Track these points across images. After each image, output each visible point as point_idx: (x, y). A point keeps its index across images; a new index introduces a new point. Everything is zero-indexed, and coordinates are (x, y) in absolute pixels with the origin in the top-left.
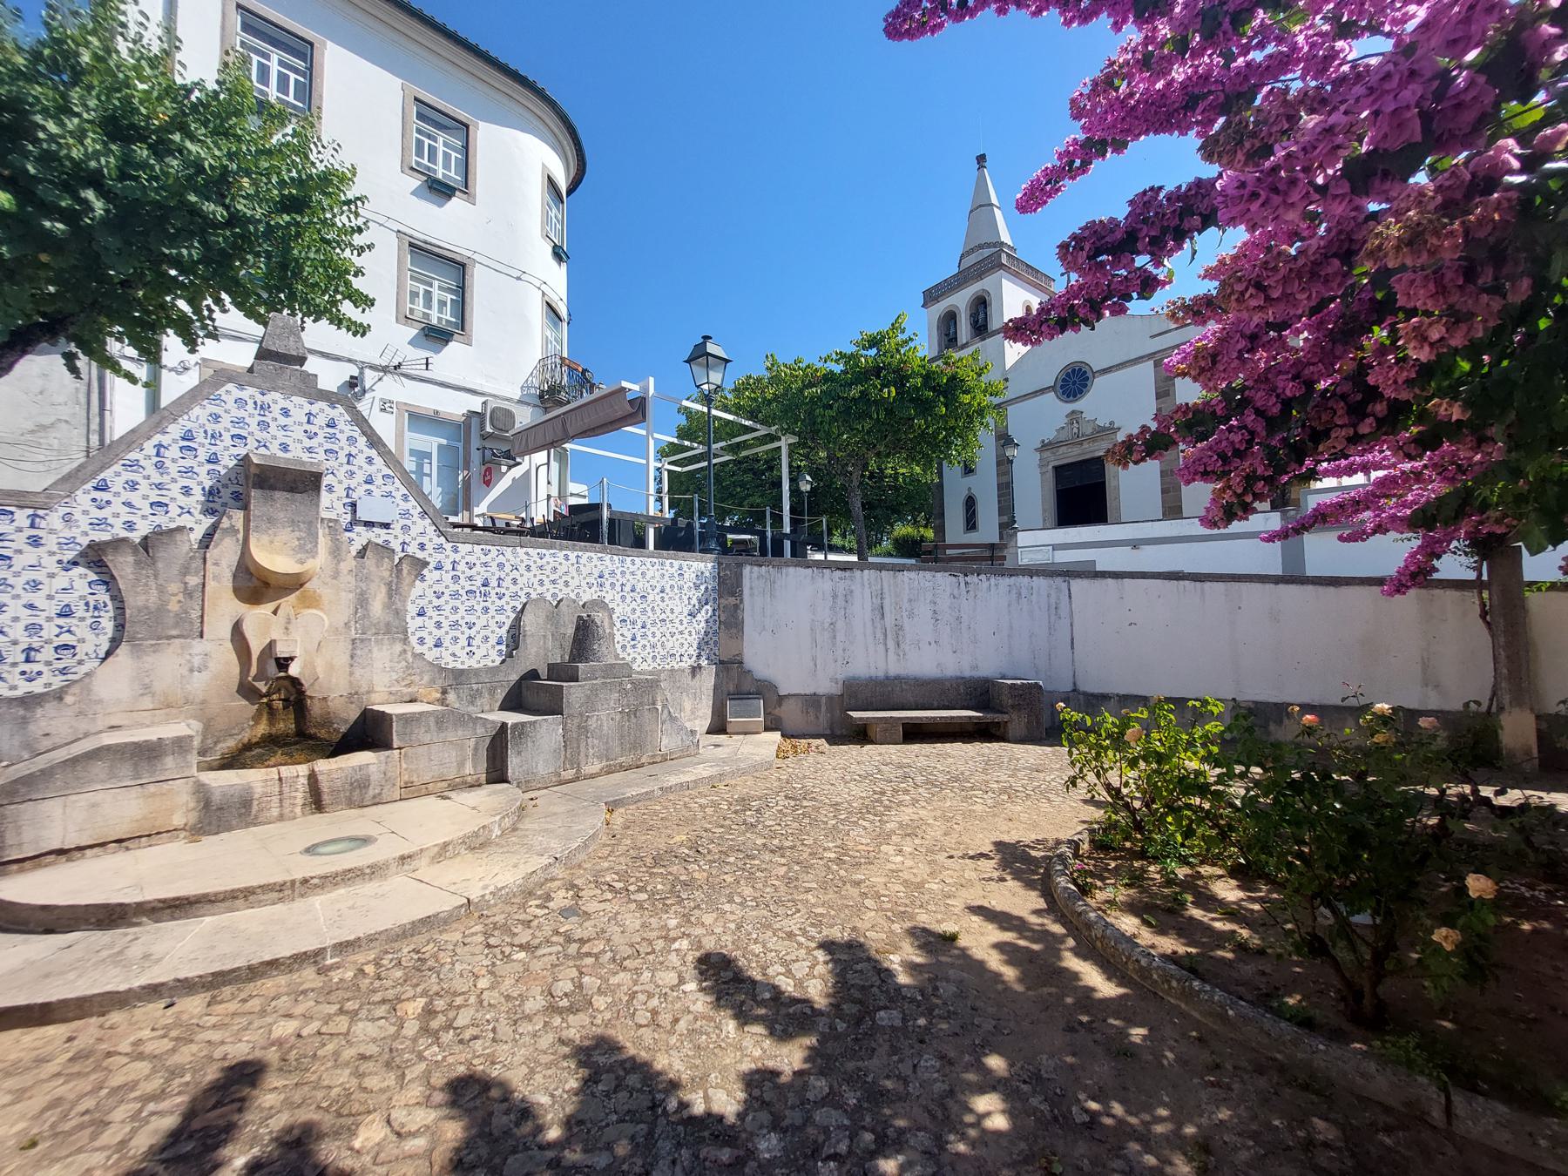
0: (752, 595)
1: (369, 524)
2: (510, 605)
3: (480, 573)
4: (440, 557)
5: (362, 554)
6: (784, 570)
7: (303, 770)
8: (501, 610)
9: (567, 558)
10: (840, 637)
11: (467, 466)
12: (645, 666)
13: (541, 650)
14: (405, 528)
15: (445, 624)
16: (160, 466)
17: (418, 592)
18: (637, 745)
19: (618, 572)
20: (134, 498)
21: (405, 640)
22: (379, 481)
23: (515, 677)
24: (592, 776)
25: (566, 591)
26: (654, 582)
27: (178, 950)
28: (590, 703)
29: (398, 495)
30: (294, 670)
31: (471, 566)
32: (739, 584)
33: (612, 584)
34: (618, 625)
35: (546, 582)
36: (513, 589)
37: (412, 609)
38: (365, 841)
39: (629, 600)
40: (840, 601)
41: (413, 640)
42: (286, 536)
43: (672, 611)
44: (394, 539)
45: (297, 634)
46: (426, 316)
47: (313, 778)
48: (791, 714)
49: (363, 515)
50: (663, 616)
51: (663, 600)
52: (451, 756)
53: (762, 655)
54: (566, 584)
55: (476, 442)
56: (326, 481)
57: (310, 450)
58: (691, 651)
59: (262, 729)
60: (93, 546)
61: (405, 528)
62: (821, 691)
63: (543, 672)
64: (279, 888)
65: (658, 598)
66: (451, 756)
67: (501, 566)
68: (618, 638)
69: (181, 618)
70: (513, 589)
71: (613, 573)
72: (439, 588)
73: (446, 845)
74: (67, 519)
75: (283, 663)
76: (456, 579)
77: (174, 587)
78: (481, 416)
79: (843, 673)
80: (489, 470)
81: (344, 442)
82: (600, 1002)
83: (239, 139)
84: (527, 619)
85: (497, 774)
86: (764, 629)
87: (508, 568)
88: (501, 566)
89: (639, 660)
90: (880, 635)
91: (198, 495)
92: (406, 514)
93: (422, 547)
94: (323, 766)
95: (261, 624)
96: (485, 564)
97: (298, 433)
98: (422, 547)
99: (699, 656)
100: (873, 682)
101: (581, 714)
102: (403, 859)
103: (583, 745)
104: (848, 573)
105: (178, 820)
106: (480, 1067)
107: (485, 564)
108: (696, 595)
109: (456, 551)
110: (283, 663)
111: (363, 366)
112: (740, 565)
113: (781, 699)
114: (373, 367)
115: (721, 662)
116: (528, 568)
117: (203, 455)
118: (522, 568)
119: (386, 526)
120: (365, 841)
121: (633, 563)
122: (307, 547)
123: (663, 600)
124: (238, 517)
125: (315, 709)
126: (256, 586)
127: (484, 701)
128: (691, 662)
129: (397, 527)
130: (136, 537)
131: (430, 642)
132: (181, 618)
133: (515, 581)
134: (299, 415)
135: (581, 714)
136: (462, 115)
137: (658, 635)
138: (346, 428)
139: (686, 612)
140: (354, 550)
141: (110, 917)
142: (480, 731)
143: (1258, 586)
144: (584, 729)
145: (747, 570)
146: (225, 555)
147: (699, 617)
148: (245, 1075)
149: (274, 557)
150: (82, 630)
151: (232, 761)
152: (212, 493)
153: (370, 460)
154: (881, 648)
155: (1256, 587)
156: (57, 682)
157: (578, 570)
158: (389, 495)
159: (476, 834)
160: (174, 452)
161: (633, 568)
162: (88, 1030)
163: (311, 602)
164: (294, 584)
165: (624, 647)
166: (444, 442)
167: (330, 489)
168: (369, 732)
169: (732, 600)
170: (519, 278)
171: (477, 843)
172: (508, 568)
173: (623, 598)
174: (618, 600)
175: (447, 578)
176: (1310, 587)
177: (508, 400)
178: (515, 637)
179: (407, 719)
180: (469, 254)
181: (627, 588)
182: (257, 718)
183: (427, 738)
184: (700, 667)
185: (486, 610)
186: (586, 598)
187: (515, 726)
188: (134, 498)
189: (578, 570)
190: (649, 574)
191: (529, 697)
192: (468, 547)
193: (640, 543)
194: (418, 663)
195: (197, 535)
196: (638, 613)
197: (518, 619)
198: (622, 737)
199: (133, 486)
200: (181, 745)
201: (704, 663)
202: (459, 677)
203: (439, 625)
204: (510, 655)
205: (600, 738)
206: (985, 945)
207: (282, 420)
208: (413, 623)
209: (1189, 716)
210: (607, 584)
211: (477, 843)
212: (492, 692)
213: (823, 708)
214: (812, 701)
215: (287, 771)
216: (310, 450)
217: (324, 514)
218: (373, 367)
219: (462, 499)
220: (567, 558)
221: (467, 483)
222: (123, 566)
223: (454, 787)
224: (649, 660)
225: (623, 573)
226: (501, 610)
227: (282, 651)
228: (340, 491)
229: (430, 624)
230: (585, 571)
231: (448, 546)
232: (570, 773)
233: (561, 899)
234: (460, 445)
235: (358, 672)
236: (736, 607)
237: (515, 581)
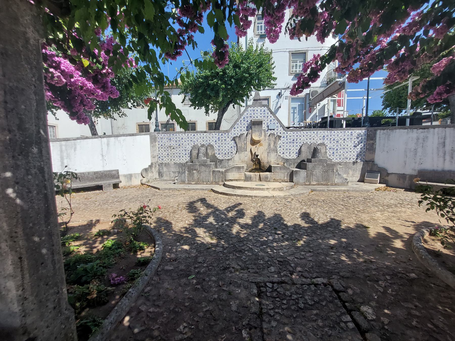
0: (380, 140)
1: (271, 130)
3: (292, 138)
4: (284, 135)
5: (269, 136)
6: (394, 131)
7: (258, 174)
8: (297, 146)
9: (314, 133)
10: (419, 154)
11: (305, 109)
12: (337, 161)
13: (306, 155)
14: (277, 130)
15: (285, 149)
16: (241, 124)
17: (280, 142)
18: (327, 180)
19: (329, 135)
20: (238, 129)
21: (277, 152)
22: (272, 121)
23: (299, 161)
24: (314, 185)
25: (313, 141)
26: (341, 137)
27: (239, 192)
28: (314, 168)
29: (276, 123)
30: (259, 157)
31: (290, 136)
33: (327, 139)
34: (328, 149)
35: (308, 139)
36: (300, 141)
37: (279, 146)
38: (264, 185)
39: (332, 142)
40: (421, 141)
41: (279, 153)
42: (257, 133)
43: (347, 145)
44: (275, 132)
45: (259, 151)
46: (296, 71)
47: (260, 175)
48: (392, 179)
49: (270, 128)
50: (344, 147)
51: (344, 142)
52: (282, 175)
53: (381, 159)
54: (314, 139)
55: (308, 102)
56: (263, 122)
57: (261, 117)
58: (354, 157)
59: (254, 167)
60: (234, 137)
61: (277, 130)
62: (407, 173)
63: (306, 160)
64: (250, 188)
65: (342, 142)
66: (282, 175)
67: (297, 136)
68: (328, 153)
69: (244, 148)
70: (300, 141)
71: (328, 136)
72: (284, 142)
73: (275, 188)
74: (231, 134)
75: (257, 156)
76: (287, 139)
77: (243, 143)
78: (309, 94)
79: (418, 167)
80: (311, 109)
81: (266, 114)
82: (283, 211)
84: (303, 148)
85: (291, 180)
86: (384, 151)
87: (299, 136)
88: (297, 136)
89: (335, 159)
90: (441, 154)
91: (246, 128)
92: (277, 127)
93: (280, 133)
94: (261, 173)
95: (253, 148)
96: (293, 136)
97: (259, 114)
98: (280, 133)
99: (357, 159)
100: (435, 172)
101: (311, 170)
102: (267, 189)
103: (311, 178)
104: (426, 130)
105: (243, 179)
106: (263, 211)
107: (293, 136)
109: (287, 133)
110: (257, 156)
111: (281, 89)
112: (376, 130)
113: (388, 174)
114: (284, 89)
115: (366, 161)
116: (304, 136)
117: (246, 121)
118: (302, 136)
119: (274, 130)
120: (264, 185)
121: (334, 132)
122: (260, 135)
123: (344, 142)
124: (251, 130)
125: (262, 164)
126: (254, 143)
127: (292, 166)
128: (354, 160)
129: (276, 129)
130: (238, 136)
131: (282, 153)
132: (244, 148)
133: (300, 139)
134: (259, 111)
135: (311, 170)
137: (342, 152)
138: (267, 111)
139: (353, 145)
140: (269, 134)
141: (233, 187)
142: (288, 171)
144: (312, 174)
145: (378, 132)
146: (249, 137)
147: (358, 147)
148: (241, 204)
149: (256, 138)
150: (233, 150)
151: (250, 171)
152: (247, 127)
153: (271, 117)
154: (441, 159)
156: (231, 157)
157: (317, 135)
158: (274, 123)
159: (280, 188)
160: (242, 121)
161: (334, 134)
162: (230, 197)
163: (261, 145)
165: (330, 155)
166: (300, 103)
167: (264, 123)
168: (269, 170)
169: (372, 142)
170: (321, 50)
171: (281, 189)
172: (299, 136)
173: (331, 142)
174: (329, 142)
175: (285, 139)
177: (317, 87)
178: (300, 152)
179: (275, 167)
180: (306, 49)
181: (332, 139)
182: (254, 165)
183: (278, 171)
184: (357, 162)
185: (293, 146)
186: (319, 142)
187: (295, 171)
188: (238, 129)
189: (317, 135)
190: (340, 135)
191: (302, 166)
192: (290, 132)
193: (341, 126)
194: (279, 157)
195: (245, 135)
196: (335, 146)
197: (301, 148)
198: (323, 177)
199: (238, 127)
200: (243, 167)
201: (359, 161)
202: (287, 160)
203: (283, 149)
204: (298, 156)
205: (316, 177)
207: (257, 112)
208: (279, 149)
210: (326, 139)
211: (281, 189)
212: (294, 164)
213: (407, 179)
214: (402, 176)
215: (256, 173)
216: (261, 117)
217: (263, 129)
218: (284, 89)
219: (304, 118)
220: (314, 133)
221: (305, 113)
222: (237, 140)
223: (283, 181)
224: (338, 159)
225: (331, 135)
226: (297, 146)
227: (257, 154)
228: (266, 124)
229: (282, 149)
230: (319, 136)
231: (286, 132)
232: (308, 182)
233: (289, 200)
234: (304, 103)
235: (269, 158)
236: (373, 144)
237: (300, 139)
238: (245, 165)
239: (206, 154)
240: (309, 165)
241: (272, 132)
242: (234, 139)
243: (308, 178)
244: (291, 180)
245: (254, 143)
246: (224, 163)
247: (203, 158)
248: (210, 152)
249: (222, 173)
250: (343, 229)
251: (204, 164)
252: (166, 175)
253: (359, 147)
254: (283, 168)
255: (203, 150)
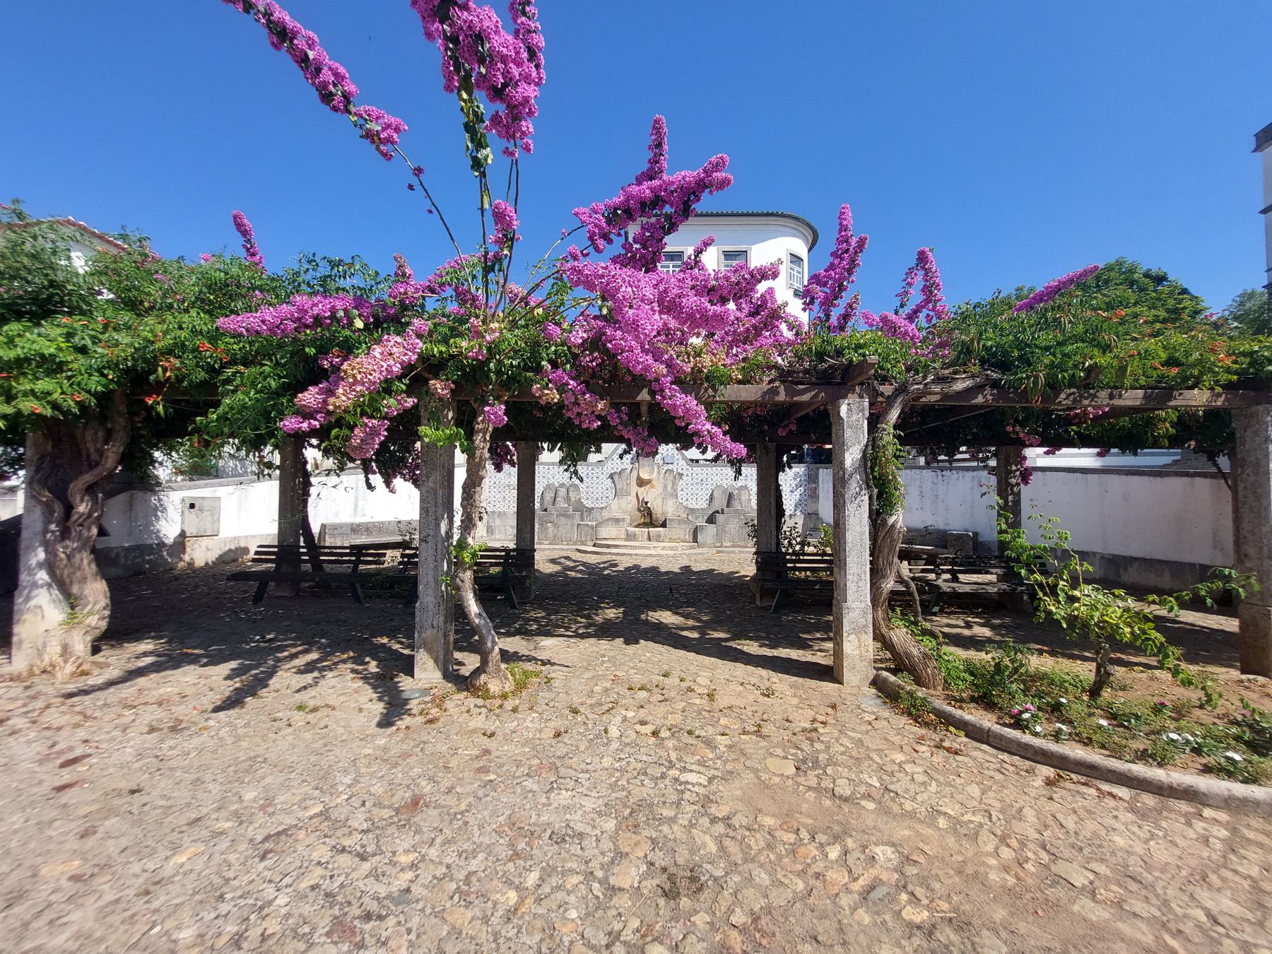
2: (710, 487)
17: (681, 483)
32: (817, 477)
42: (647, 469)
83: (90, 305)
108: (794, 483)
126: (641, 483)
136: (743, 248)
141: (608, 546)
143: (1117, 477)
145: (821, 471)
146: (635, 473)
149: (645, 476)
155: (1116, 477)
163: (653, 487)
164: (649, 482)
176: (1146, 478)
178: (711, 498)
201: (798, 513)
206: (372, 728)
209: (631, 822)
222: (616, 478)
238: (628, 518)
239: (568, 499)
240: (720, 517)
241: (670, 467)
242: (611, 476)
243: (719, 537)
244: (695, 540)
245: (641, 483)
246: (595, 514)
247: (562, 504)
248: (573, 496)
249: (592, 527)
250: (1073, 913)
251: (564, 514)
252: (500, 532)
253: (797, 493)
254: (688, 521)
255: (562, 492)
